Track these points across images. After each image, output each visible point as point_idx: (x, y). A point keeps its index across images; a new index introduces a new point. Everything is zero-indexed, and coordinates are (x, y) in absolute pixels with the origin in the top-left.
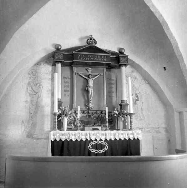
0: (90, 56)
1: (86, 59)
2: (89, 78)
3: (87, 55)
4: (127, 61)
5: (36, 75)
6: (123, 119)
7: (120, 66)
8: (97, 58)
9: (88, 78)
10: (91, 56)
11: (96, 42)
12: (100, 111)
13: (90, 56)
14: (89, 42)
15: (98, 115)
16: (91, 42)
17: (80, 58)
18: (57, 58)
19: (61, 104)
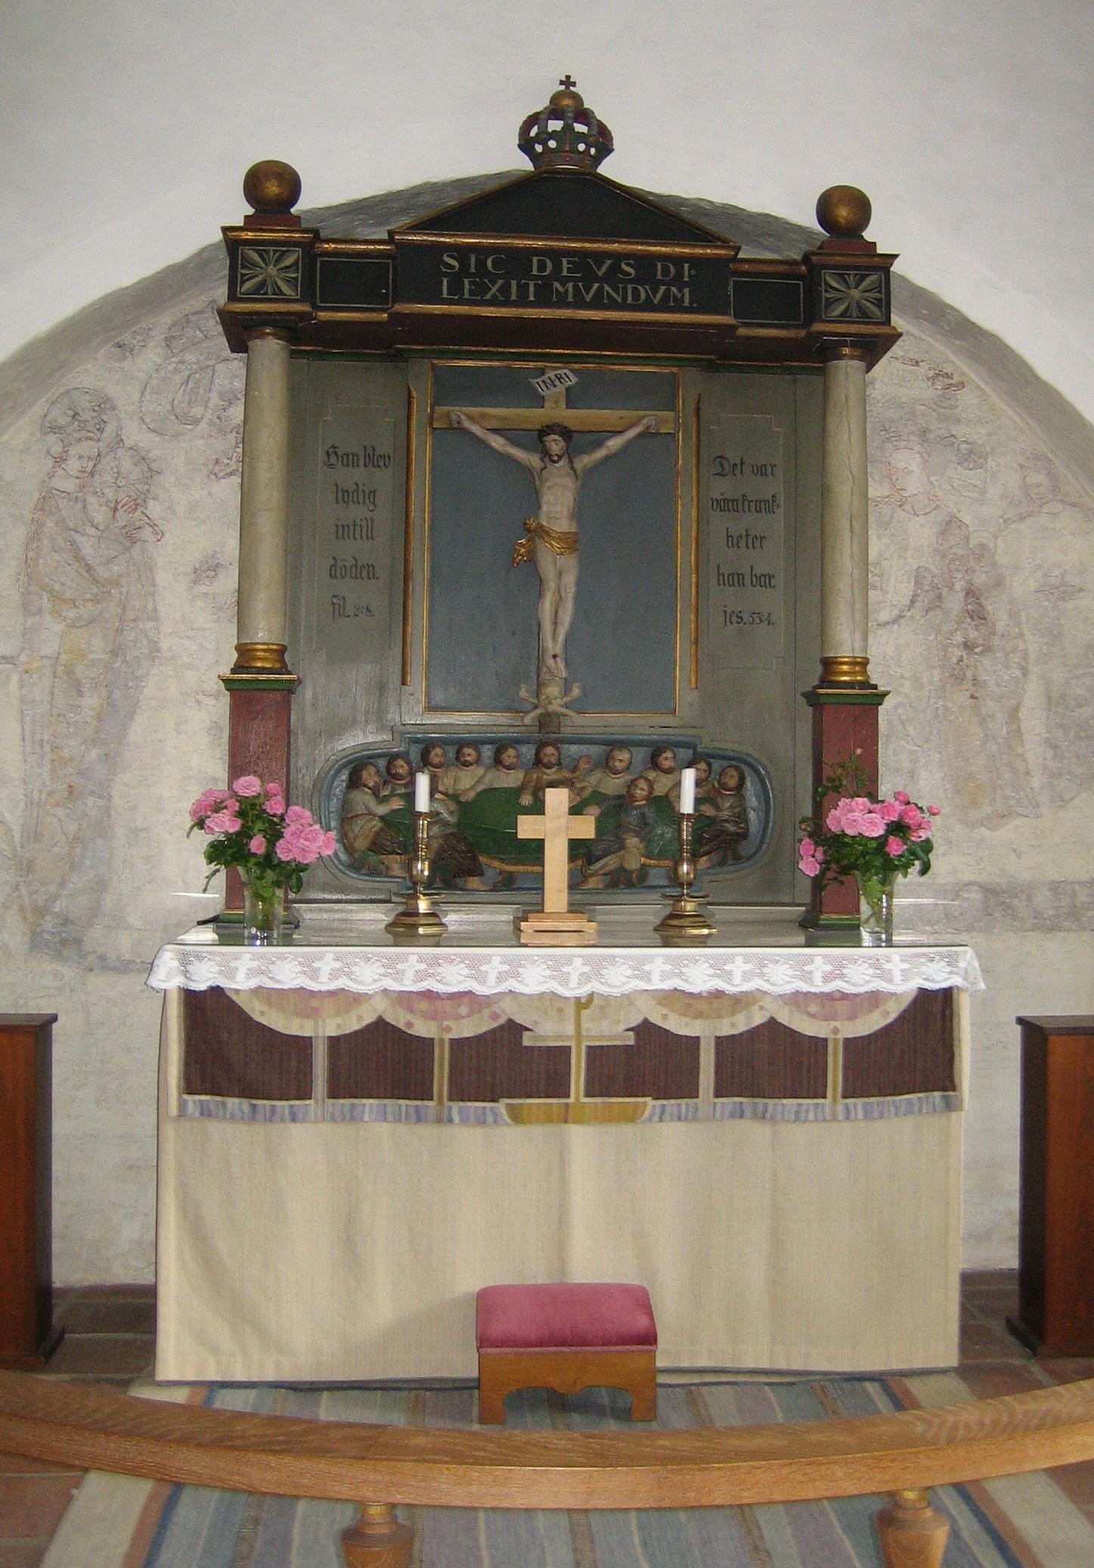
0: (542, 266)
1: (505, 290)
2: (545, 453)
3: (516, 262)
4: (885, 304)
5: (110, 429)
6: (601, 886)
7: (820, 354)
8: (614, 277)
9: (534, 460)
10: (557, 266)
11: (603, 142)
12: (640, 744)
13: (542, 266)
14: (538, 139)
15: (628, 777)
16: (554, 135)
17: (456, 288)
18: (289, 261)
19: (291, 692)
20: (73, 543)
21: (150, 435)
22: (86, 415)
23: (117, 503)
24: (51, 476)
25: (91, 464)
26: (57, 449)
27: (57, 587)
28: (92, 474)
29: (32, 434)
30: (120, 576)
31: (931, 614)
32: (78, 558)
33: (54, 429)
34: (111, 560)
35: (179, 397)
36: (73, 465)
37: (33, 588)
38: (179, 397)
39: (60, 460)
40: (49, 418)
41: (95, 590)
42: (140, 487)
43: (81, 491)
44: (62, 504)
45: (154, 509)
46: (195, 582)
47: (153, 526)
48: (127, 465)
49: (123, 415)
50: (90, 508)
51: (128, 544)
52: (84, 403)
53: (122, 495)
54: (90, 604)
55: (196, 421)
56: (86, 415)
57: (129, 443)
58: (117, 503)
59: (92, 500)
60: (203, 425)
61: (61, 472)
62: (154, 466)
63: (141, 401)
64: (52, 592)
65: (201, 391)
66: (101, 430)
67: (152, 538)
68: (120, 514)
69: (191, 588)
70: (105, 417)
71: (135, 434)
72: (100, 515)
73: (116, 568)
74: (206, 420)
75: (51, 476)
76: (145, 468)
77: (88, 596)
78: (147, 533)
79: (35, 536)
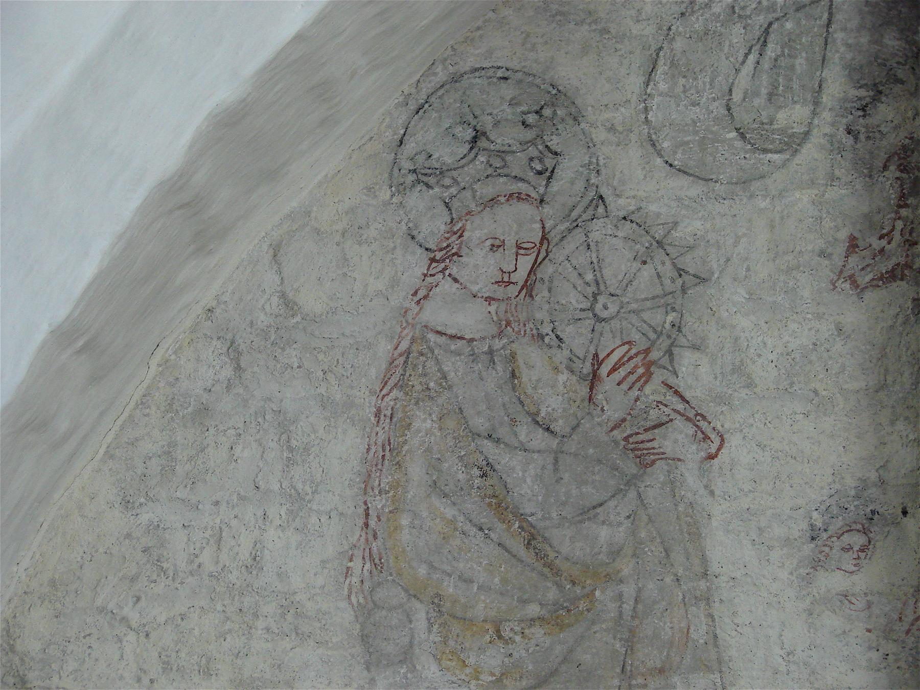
5: (569, 171)
20: (487, 470)
21: (681, 183)
22: (507, 137)
23: (597, 362)
24: (421, 297)
25: (525, 263)
26: (434, 227)
27: (450, 588)
28: (528, 287)
29: (370, 190)
30: (616, 553)
31: (492, 138)
32: (501, 505)
33: (425, 175)
34: (589, 512)
35: (743, 81)
36: (479, 267)
37: (391, 594)
38: (743, 81)
39: (443, 257)
40: (410, 147)
41: (552, 594)
42: (657, 318)
43: (500, 334)
44: (455, 367)
45: (696, 374)
46: (816, 564)
47: (697, 419)
48: (618, 262)
49: (600, 135)
50: (527, 377)
51: (631, 468)
52: (498, 104)
53: (608, 343)
54: (538, 632)
55: (793, 143)
56: (502, 138)
57: (619, 205)
58: (597, 362)
59: (535, 362)
60: (811, 152)
61: (447, 285)
62: (689, 262)
63: (645, 97)
64: (437, 602)
65: (800, 63)
66: (549, 175)
67: (693, 453)
68: (608, 385)
69: (808, 580)
70: (554, 142)
71: (640, 183)
72: (555, 394)
73: (604, 533)
74: (817, 138)
75: (421, 297)
76: (668, 270)
77: (533, 610)
78: (678, 439)
79: (387, 454)
